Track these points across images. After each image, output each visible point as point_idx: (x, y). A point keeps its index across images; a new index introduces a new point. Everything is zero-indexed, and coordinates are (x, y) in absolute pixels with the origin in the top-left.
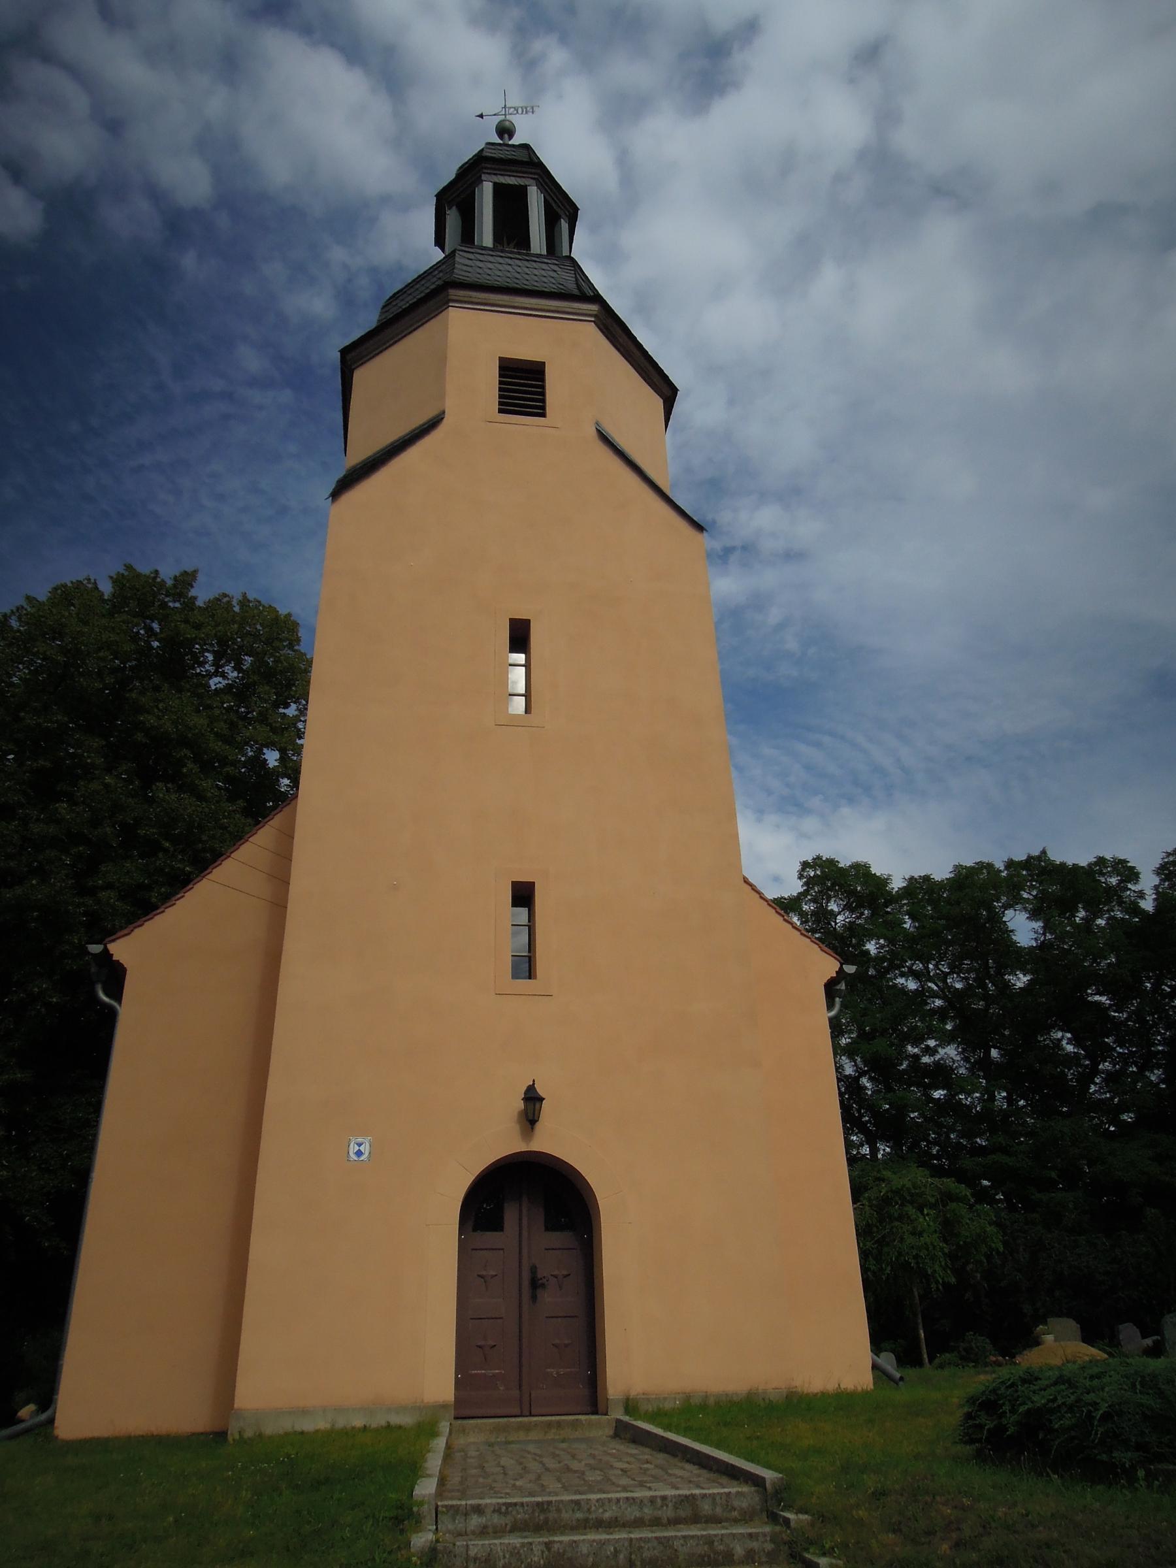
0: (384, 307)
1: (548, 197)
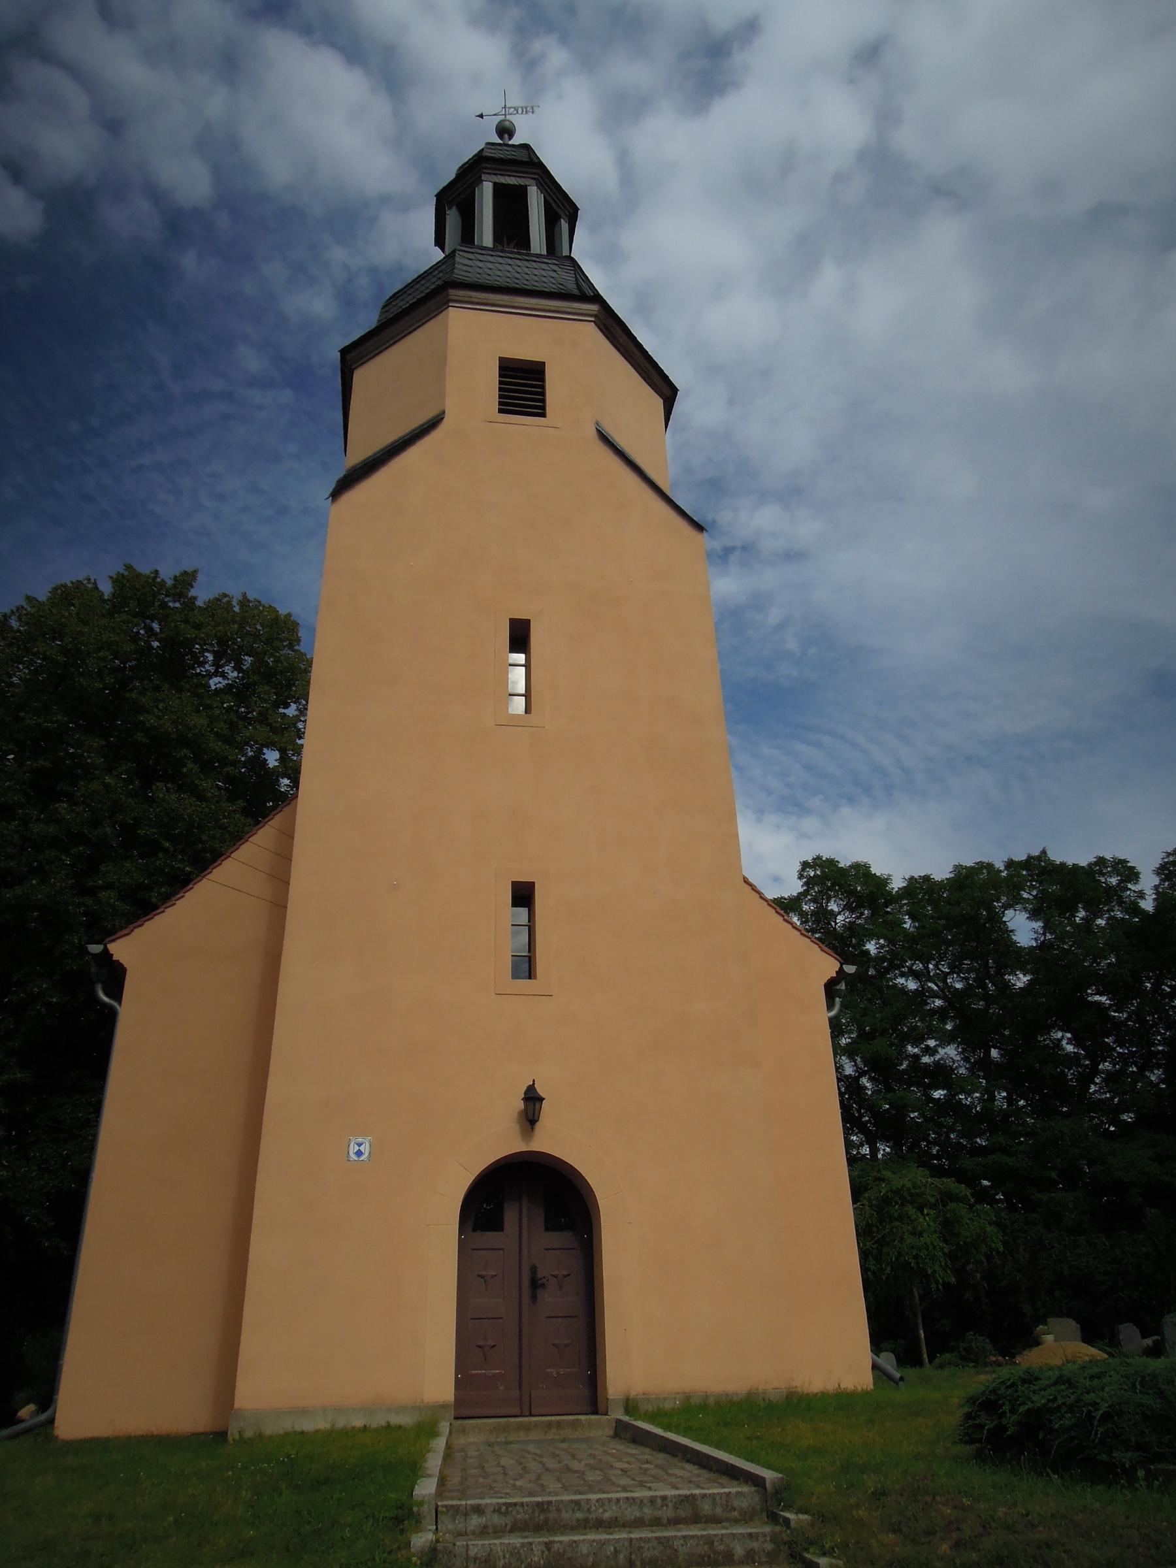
0: (384, 307)
1: (548, 197)
